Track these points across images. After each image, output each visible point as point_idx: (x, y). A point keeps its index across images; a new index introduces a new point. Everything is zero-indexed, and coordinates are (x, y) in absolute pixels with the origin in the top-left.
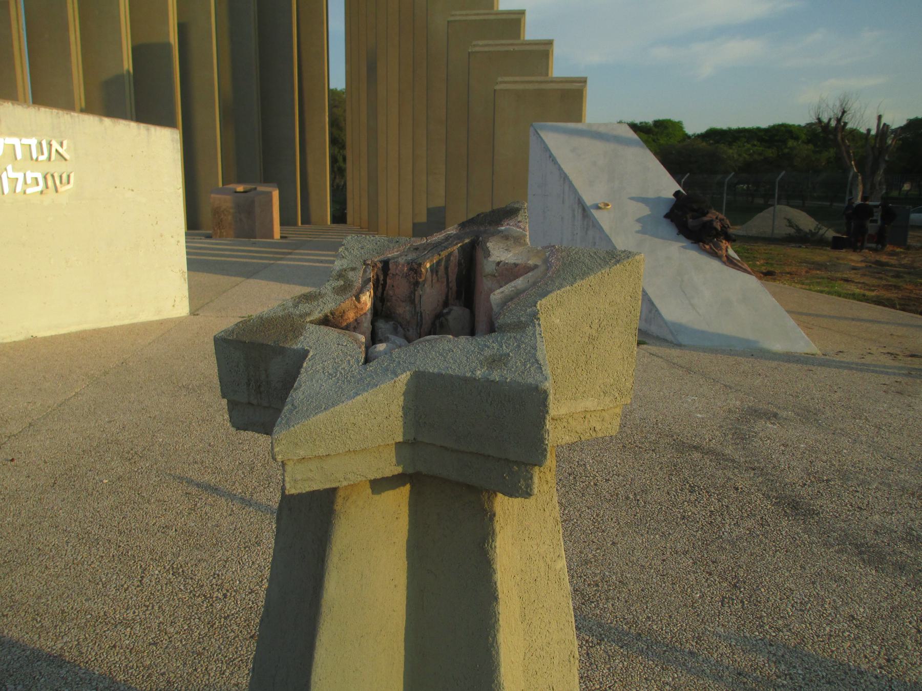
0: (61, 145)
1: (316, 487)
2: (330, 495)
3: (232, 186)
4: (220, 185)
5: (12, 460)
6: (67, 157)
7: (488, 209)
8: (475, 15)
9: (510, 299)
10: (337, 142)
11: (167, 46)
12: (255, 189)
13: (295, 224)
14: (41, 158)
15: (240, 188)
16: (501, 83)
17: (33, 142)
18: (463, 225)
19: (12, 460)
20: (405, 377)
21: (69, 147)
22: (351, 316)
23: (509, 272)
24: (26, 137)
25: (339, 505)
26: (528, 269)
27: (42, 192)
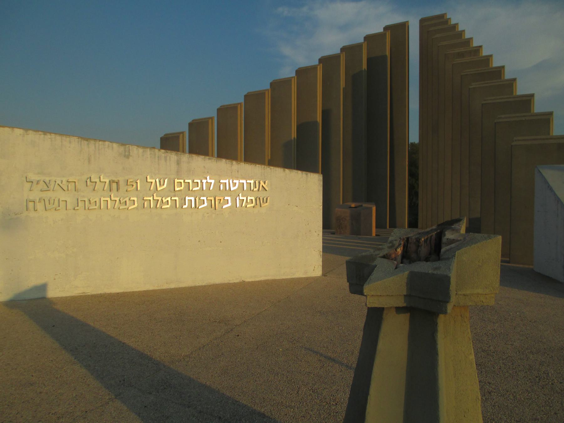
0: (265, 183)
1: (376, 306)
2: (382, 309)
3: (349, 204)
4: (341, 203)
5: (238, 336)
6: (267, 189)
7: (450, 219)
8: (500, 99)
9: (448, 250)
10: (413, 175)
11: (316, 123)
12: (362, 206)
13: (386, 228)
14: (255, 189)
15: (353, 205)
16: (516, 140)
17: (252, 182)
18: (439, 225)
19: (238, 336)
20: (407, 273)
21: (268, 184)
22: (393, 256)
23: (451, 241)
24: (249, 180)
25: (384, 316)
26: (458, 241)
27: (254, 207)
